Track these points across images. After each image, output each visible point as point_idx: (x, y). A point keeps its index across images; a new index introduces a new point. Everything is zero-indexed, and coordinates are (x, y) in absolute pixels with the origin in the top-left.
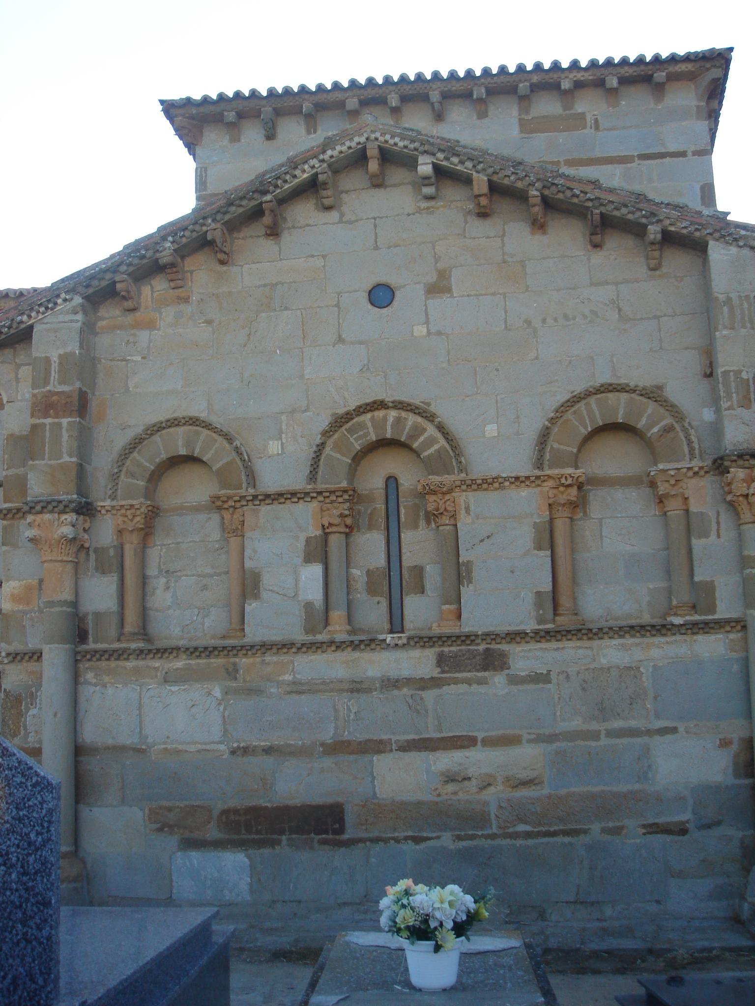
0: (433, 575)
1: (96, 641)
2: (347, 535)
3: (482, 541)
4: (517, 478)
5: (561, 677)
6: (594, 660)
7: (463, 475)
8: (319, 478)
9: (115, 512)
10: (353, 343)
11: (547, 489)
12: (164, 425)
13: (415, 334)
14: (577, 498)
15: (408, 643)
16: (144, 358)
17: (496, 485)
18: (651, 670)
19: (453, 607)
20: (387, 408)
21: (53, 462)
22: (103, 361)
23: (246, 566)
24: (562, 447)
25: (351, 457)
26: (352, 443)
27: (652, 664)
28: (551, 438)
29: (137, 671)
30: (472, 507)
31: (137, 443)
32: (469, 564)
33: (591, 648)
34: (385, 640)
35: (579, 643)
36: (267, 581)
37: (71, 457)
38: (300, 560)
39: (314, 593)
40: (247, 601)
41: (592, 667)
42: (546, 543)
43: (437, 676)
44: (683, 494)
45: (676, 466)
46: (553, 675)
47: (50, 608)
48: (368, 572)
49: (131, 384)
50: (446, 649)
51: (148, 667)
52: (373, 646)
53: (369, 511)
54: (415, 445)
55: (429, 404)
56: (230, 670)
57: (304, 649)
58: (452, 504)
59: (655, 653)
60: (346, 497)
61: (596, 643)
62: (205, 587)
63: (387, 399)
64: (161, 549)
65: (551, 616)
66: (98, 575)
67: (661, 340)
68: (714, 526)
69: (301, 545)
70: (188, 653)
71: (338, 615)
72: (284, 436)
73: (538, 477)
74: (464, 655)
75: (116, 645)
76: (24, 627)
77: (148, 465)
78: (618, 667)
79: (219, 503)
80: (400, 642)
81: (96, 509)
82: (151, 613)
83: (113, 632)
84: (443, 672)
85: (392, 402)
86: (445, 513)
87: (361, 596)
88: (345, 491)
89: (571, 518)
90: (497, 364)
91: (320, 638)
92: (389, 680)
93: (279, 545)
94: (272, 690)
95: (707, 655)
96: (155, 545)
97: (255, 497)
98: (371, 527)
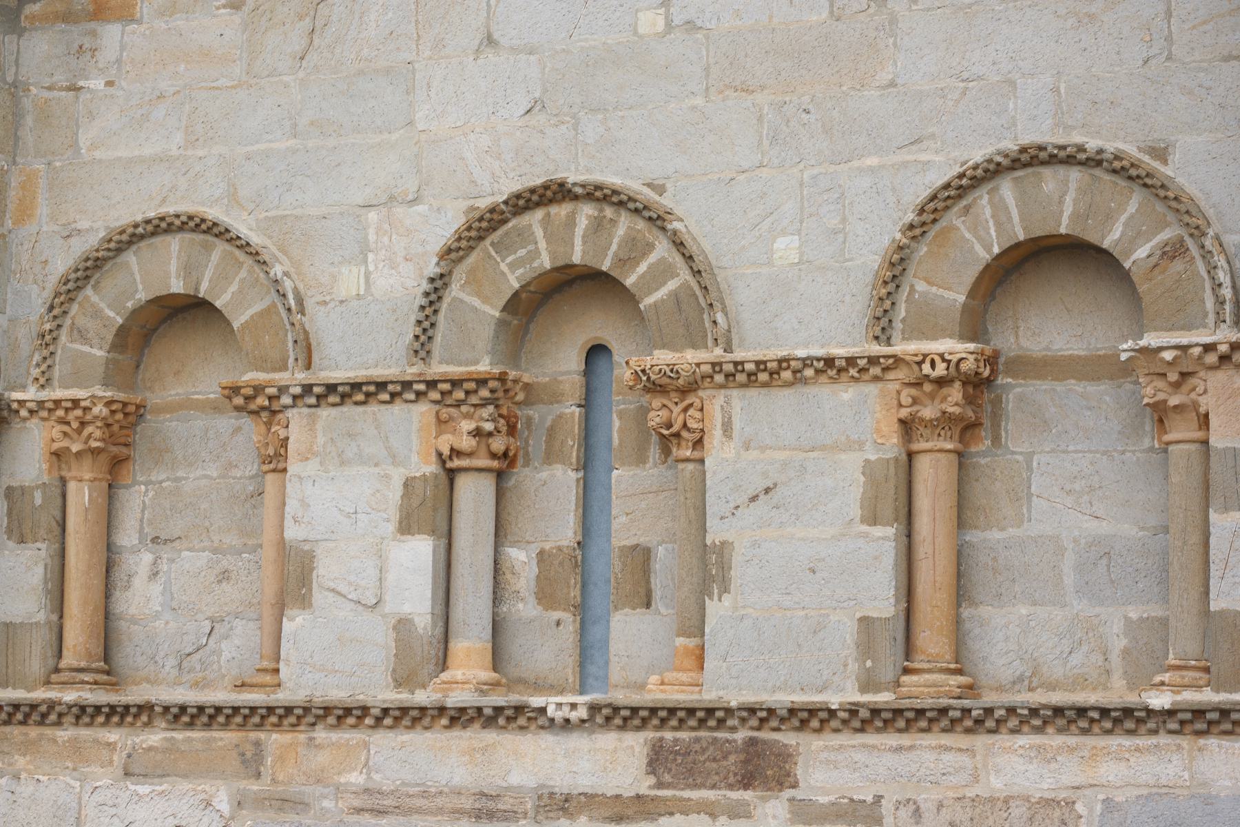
0: (667, 564)
2: (500, 475)
3: (754, 499)
4: (829, 362)
5: (904, 813)
6: (976, 779)
7: (718, 351)
8: (437, 346)
9: (44, 414)
10: (514, 50)
11: (897, 386)
12: (140, 230)
13: (641, 31)
14: (968, 408)
15: (591, 718)
16: (110, 84)
17: (787, 375)
18: (1099, 808)
19: (692, 642)
20: (576, 198)
22: (34, 90)
23: (286, 535)
24: (934, 289)
25: (502, 302)
26: (503, 273)
27: (1101, 797)
28: (911, 271)
29: (75, 747)
30: (737, 424)
31: (91, 268)
32: (723, 549)
33: (970, 751)
34: (543, 710)
35: (946, 739)
36: (326, 570)
38: (391, 527)
39: (414, 599)
40: (288, 612)
41: (970, 793)
43: (647, 792)
44: (1195, 405)
45: (1175, 341)
46: (887, 806)
48: (541, 553)
49: (84, 140)
50: (669, 735)
51: (96, 741)
52: (522, 721)
53: (548, 423)
54: (629, 281)
55: (660, 190)
56: (249, 755)
57: (388, 721)
58: (698, 415)
59: (1109, 771)
60: (484, 393)
61: (981, 741)
62: (225, 576)
63: (571, 180)
66: (11, 544)
67: (1169, 39)
69: (395, 494)
70: (170, 717)
71: (470, 646)
72: (371, 256)
73: (873, 361)
74: (704, 750)
75: (40, 694)
77: (111, 314)
78: (1027, 799)
79: (239, 401)
80: (574, 716)
82: (123, 625)
83: (36, 666)
84: (660, 785)
85: (583, 186)
86: (685, 434)
87: (524, 608)
88: (482, 382)
89: (960, 454)
90: (807, 98)
91: (422, 697)
92: (552, 794)
93: (350, 496)
94: (326, 804)
95: (1228, 783)
96: (135, 483)
97: (308, 389)
98: (550, 457)
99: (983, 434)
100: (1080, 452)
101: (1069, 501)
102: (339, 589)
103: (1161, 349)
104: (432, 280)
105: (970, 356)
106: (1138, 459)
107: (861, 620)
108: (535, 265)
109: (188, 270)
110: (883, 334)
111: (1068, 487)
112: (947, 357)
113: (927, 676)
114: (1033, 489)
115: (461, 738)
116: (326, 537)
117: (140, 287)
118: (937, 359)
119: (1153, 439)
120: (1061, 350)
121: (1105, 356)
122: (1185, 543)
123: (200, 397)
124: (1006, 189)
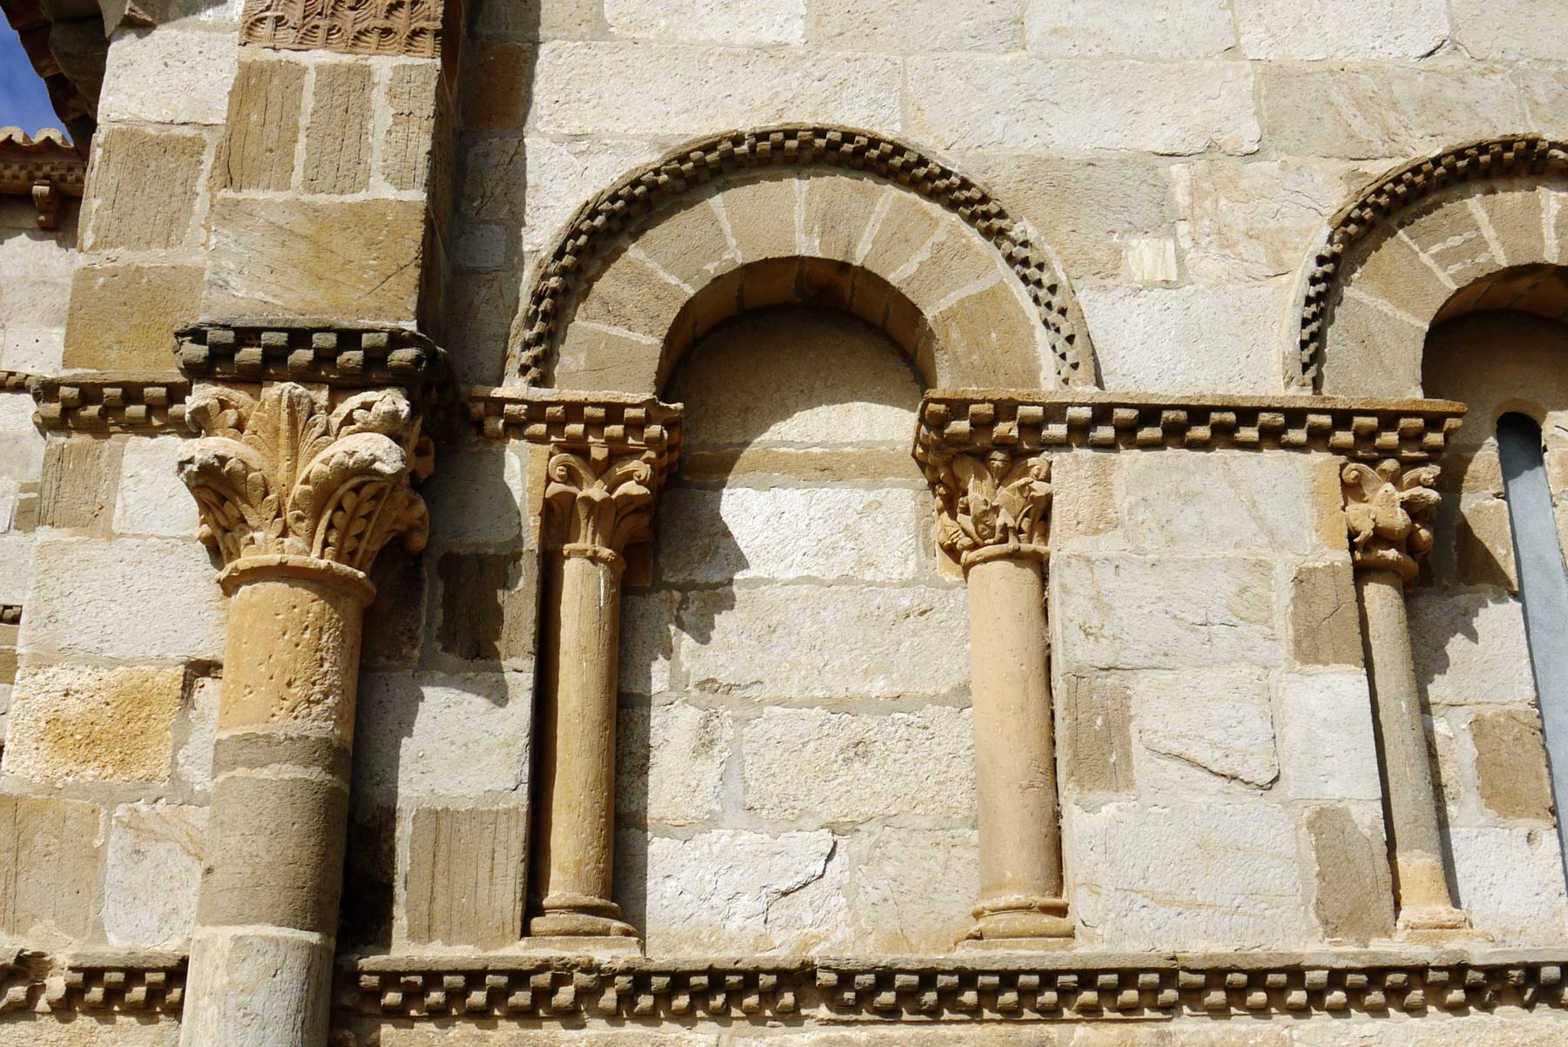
1: (424, 932)
21: (322, 199)
37: (401, 185)
38: (1284, 649)
47: (251, 764)
62: (860, 749)
64: (685, 600)
72: (1183, 228)
75: (519, 952)
76: (97, 856)
81: (465, 412)
96: (659, 585)
102: (1191, 754)
104: (1321, 260)
108: (1481, 259)
109: (827, 222)
115: (1482, 1026)
116: (1155, 662)
117: (732, 242)
123: (792, 450)
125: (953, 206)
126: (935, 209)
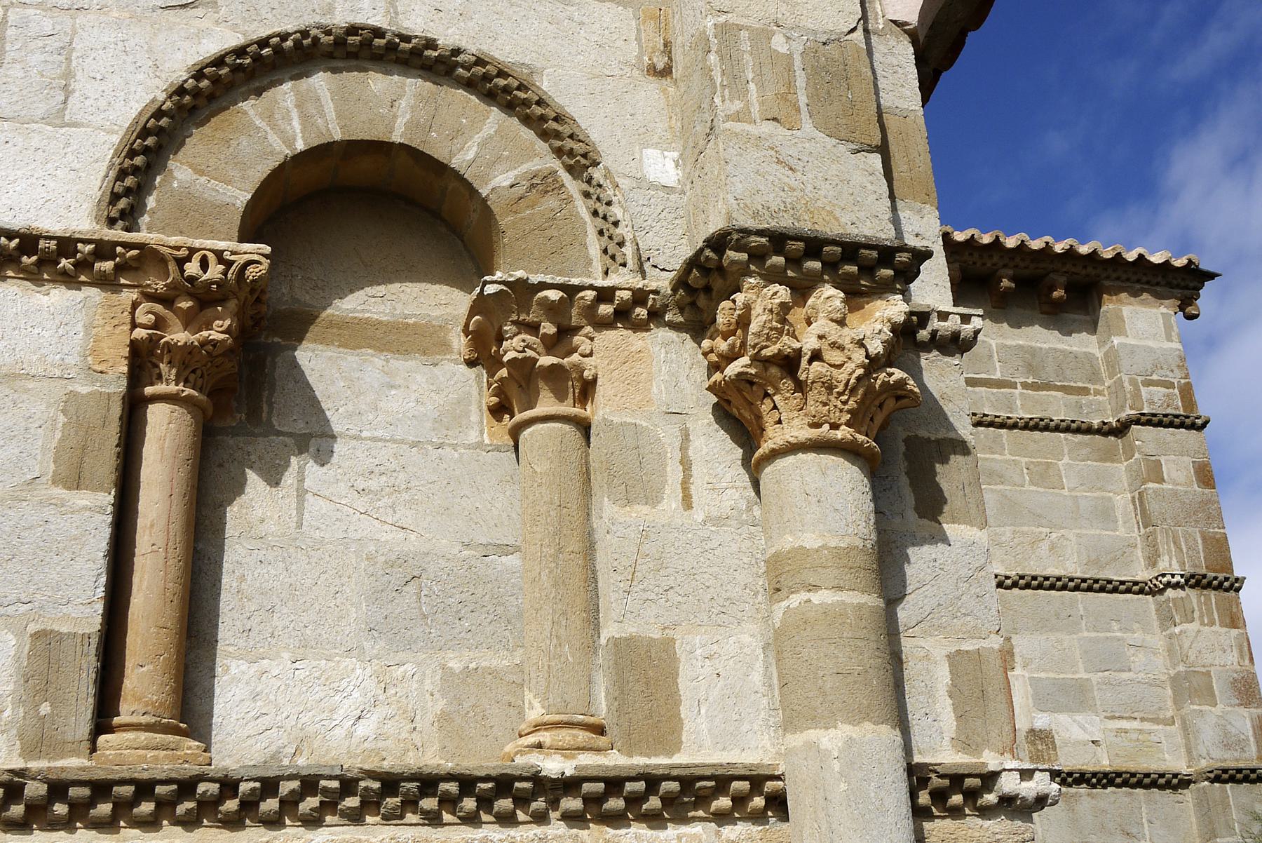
42: (106, 461)
65: (82, 723)
68: (674, 473)
99: (235, 404)
100: (380, 440)
101: (362, 504)
103: (544, 286)
105: (263, 260)
106: (461, 455)
107: (37, 636)
110: (129, 217)
111: (361, 484)
112: (227, 256)
113: (130, 735)
114: (307, 484)
118: (212, 258)
119: (482, 433)
120: (354, 310)
121: (415, 324)
122: (560, 550)
124: (320, 82)
125: (545, 135)
126: (528, 134)
